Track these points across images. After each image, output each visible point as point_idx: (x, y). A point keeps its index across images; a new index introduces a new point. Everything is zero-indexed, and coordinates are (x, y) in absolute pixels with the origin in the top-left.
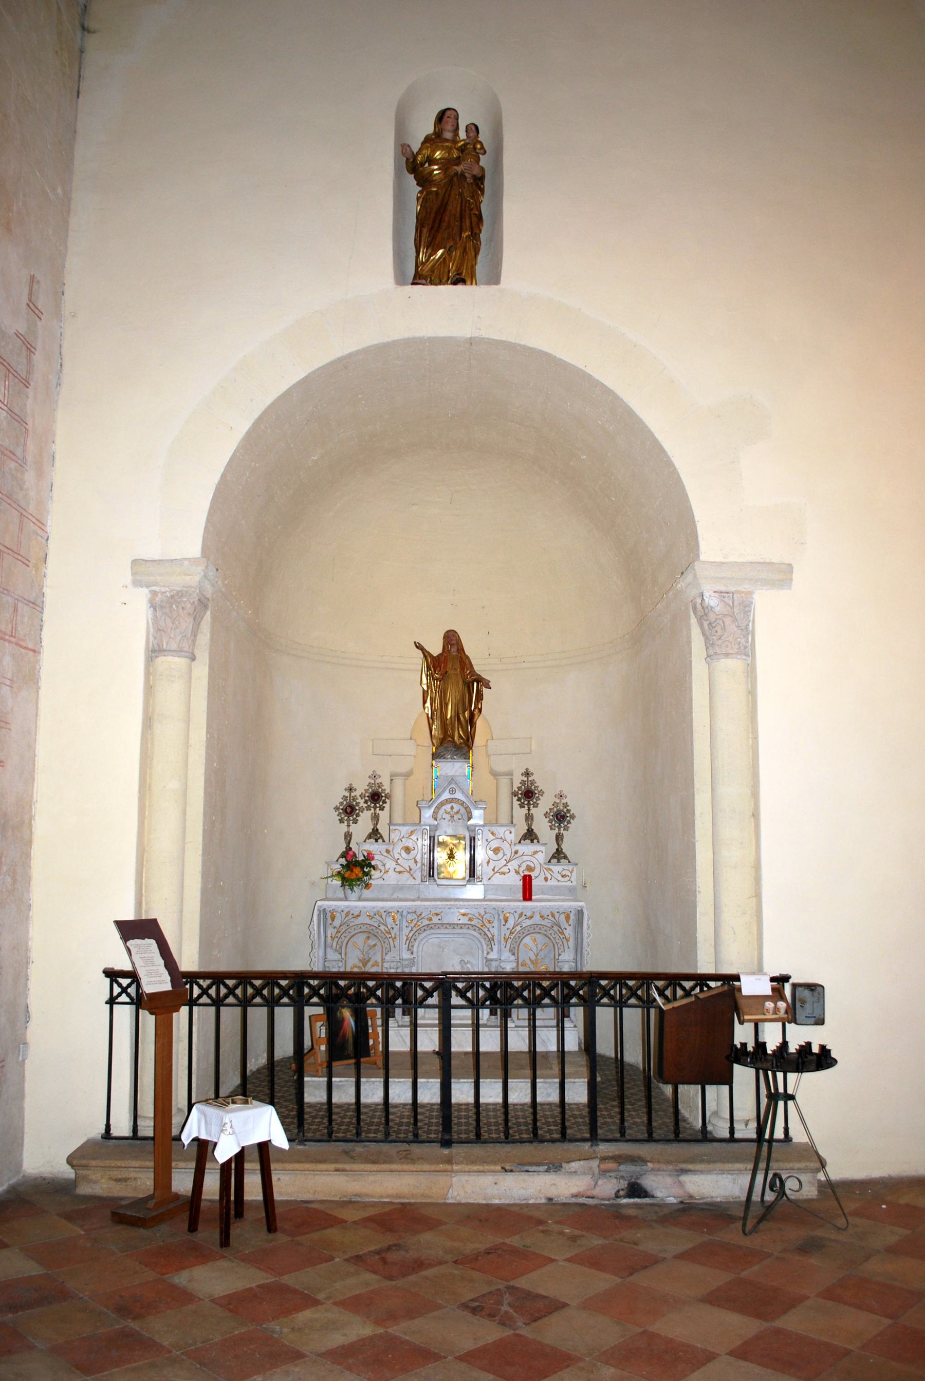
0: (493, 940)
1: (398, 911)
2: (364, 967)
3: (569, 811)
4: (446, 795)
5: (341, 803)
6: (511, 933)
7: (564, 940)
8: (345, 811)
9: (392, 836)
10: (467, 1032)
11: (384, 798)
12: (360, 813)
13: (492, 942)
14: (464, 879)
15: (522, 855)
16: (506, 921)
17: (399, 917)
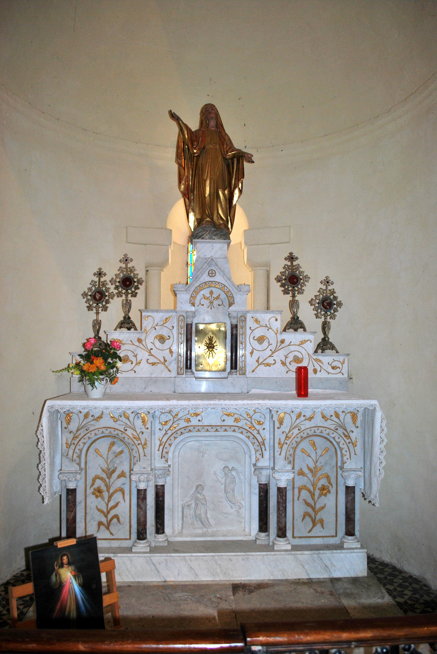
0: (264, 444)
1: (149, 412)
2: (109, 478)
3: (335, 298)
4: (205, 278)
5: (90, 289)
6: (286, 437)
7: (350, 445)
8: (94, 297)
9: (145, 323)
10: (234, 558)
11: (136, 284)
12: (111, 300)
13: (262, 446)
14: (224, 370)
15: (289, 345)
16: (281, 423)
17: (151, 419)
